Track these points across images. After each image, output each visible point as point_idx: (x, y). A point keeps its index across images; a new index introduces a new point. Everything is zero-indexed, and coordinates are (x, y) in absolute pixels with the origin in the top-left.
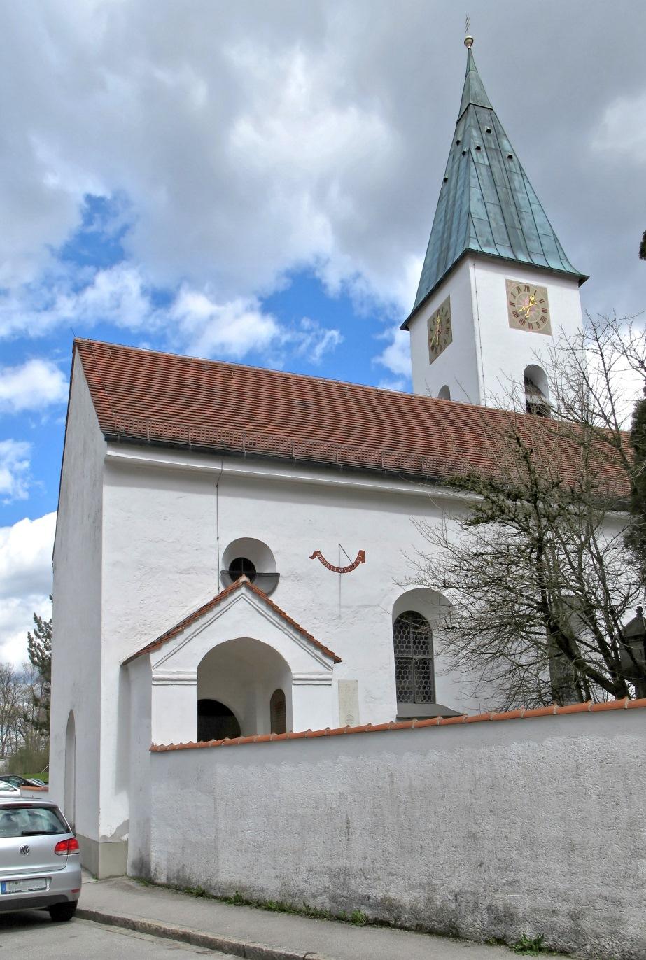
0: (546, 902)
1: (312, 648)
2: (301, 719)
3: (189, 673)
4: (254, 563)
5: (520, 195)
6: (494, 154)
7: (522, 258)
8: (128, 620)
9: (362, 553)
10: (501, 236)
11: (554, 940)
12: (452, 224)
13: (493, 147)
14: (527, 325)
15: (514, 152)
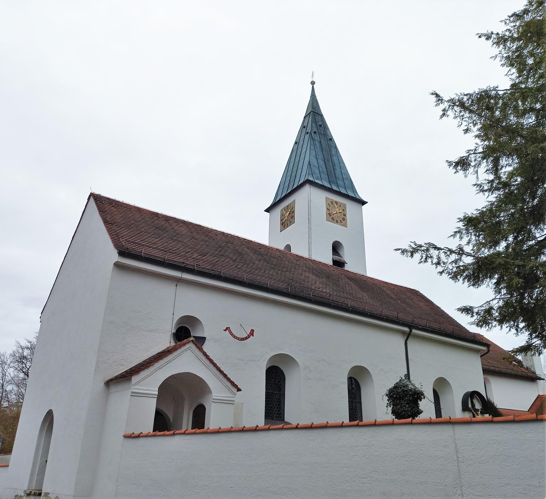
2: (214, 418)
5: (335, 158)
6: (322, 137)
7: (335, 188)
9: (252, 331)
10: (324, 176)
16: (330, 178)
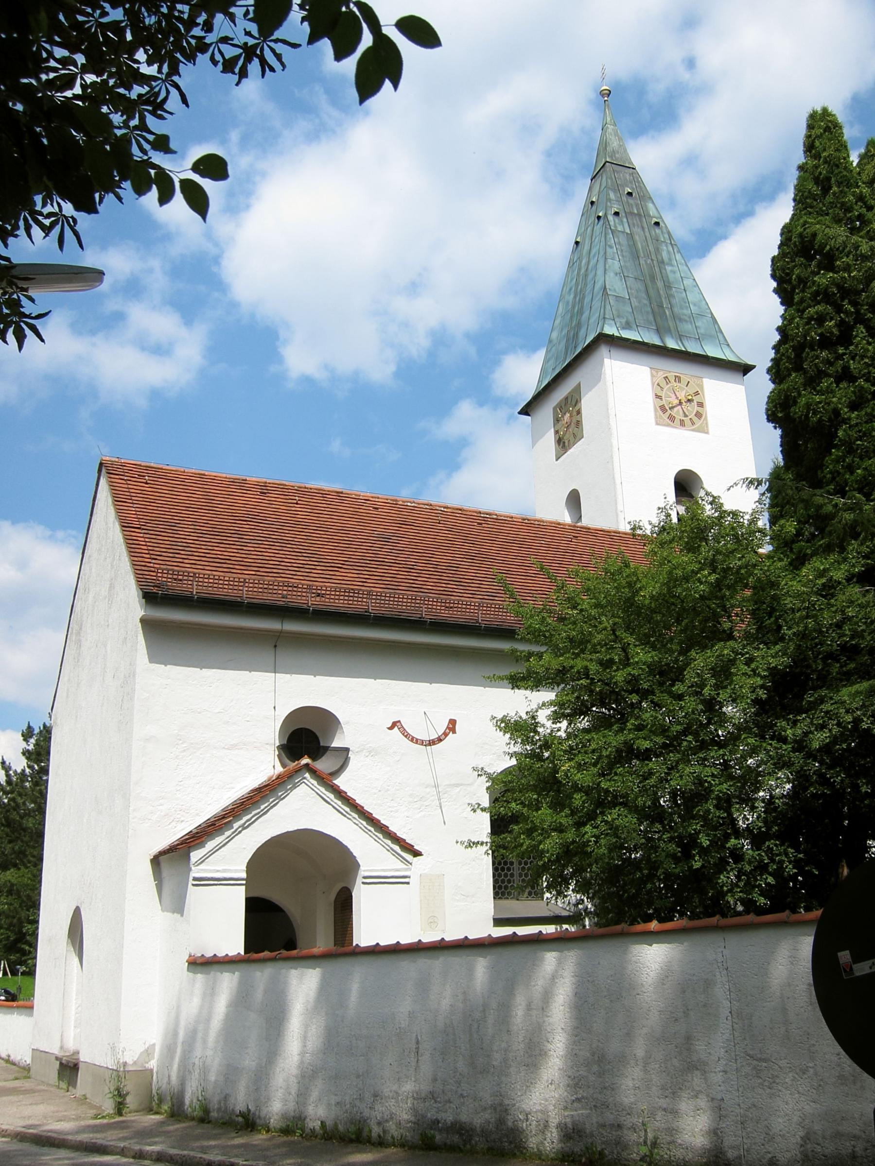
0: (612, 1117)
1: (389, 842)
2: (367, 931)
3: (236, 871)
4: (318, 734)
5: (669, 268)
6: (636, 220)
7: (672, 344)
8: (162, 805)
9: (453, 723)
11: (618, 1153)
12: (584, 298)
13: (636, 212)
14: (677, 422)
15: (661, 218)
16: (658, 319)
